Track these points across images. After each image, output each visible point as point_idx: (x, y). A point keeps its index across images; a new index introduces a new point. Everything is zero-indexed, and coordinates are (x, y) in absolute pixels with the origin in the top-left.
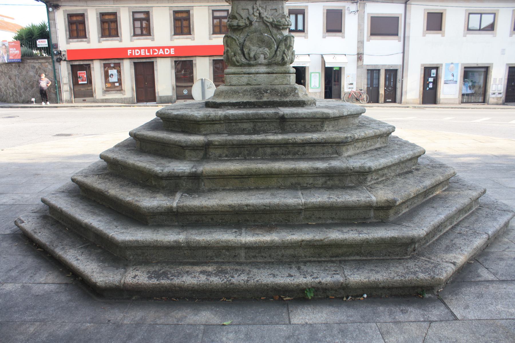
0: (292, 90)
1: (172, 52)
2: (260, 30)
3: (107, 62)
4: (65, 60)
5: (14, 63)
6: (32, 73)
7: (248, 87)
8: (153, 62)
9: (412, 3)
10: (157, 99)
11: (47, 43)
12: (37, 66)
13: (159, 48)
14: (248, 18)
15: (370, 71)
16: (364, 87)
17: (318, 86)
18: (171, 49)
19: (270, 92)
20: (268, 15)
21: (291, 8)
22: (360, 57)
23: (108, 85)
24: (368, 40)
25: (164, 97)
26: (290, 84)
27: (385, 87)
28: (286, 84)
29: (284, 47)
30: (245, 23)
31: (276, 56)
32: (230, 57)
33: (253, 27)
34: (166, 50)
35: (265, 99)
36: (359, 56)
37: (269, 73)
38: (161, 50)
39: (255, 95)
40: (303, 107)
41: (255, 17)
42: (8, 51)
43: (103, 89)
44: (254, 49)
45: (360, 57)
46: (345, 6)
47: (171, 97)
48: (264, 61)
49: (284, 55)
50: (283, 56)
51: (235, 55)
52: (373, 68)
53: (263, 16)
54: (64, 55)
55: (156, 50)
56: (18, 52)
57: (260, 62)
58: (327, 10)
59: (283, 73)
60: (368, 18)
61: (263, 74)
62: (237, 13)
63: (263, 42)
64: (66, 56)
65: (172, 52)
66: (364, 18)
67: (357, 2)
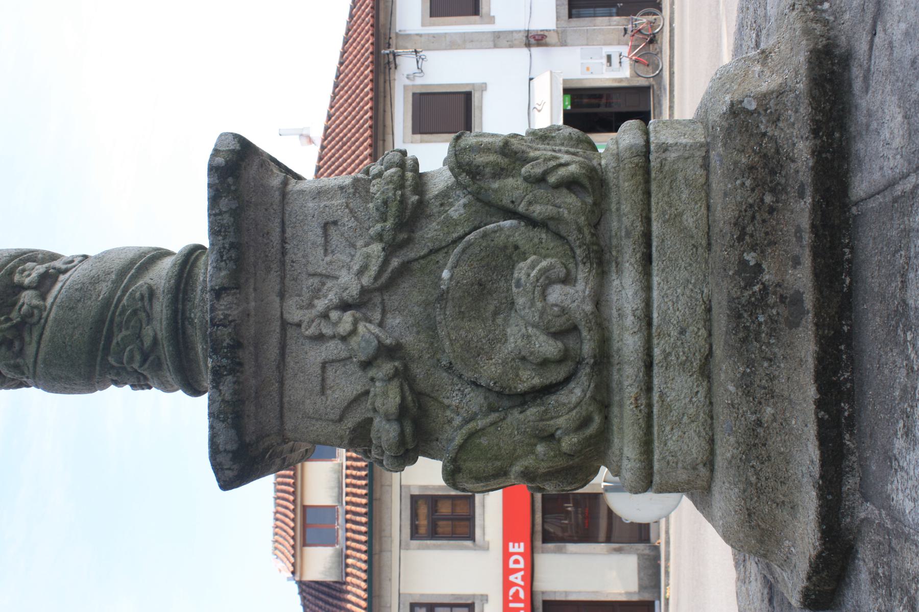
0: (745, 129)
1: (518, 548)
2: (426, 304)
7: (726, 373)
8: (546, 603)
10: (647, 597)
13: (507, 585)
14: (366, 365)
15: (574, 11)
16: (616, 23)
18: (511, 550)
19: (753, 248)
20: (350, 266)
22: (535, 40)
24: (491, 20)
25: (640, 579)
26: (707, 147)
28: (706, 165)
29: (510, 182)
30: (390, 379)
31: (558, 219)
32: (561, 463)
33: (409, 339)
34: (512, 565)
35: (802, 279)
36: (532, 41)
37: (647, 259)
38: (512, 578)
39: (773, 332)
40: (846, 59)
41: (361, 328)
44: (522, 335)
45: (535, 40)
46: (405, 87)
47: (641, 557)
48: (580, 285)
49: (552, 179)
50: (557, 186)
51: (550, 438)
53: (354, 290)
55: (512, 591)
57: (589, 307)
58: (414, 132)
59: (647, 181)
60: (434, 25)
61: (648, 288)
62: (341, 419)
63: (485, 291)
65: (518, 548)
66: (434, 36)
67: (395, 55)
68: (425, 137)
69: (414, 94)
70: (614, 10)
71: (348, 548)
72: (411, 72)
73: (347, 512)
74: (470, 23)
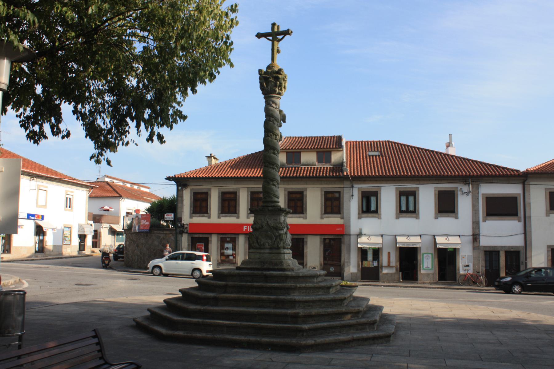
3: (224, 236)
4: (186, 233)
5: (143, 232)
6: (156, 243)
9: (531, 183)
11: (173, 216)
12: (162, 236)
17: (431, 268)
20: (271, 223)
21: (402, 190)
22: (476, 237)
23: (223, 258)
24: (484, 221)
27: (506, 270)
35: (265, 267)
42: (139, 222)
43: (218, 261)
45: (476, 237)
46: (457, 188)
52: (492, 249)
54: (186, 228)
56: (148, 223)
58: (439, 191)
60: (483, 199)
64: (188, 229)
66: (478, 199)
68: (437, 195)
69: (454, 191)
70: (488, 268)
71: (286, 168)
72: (463, 190)
73: (298, 168)
74: (483, 213)
